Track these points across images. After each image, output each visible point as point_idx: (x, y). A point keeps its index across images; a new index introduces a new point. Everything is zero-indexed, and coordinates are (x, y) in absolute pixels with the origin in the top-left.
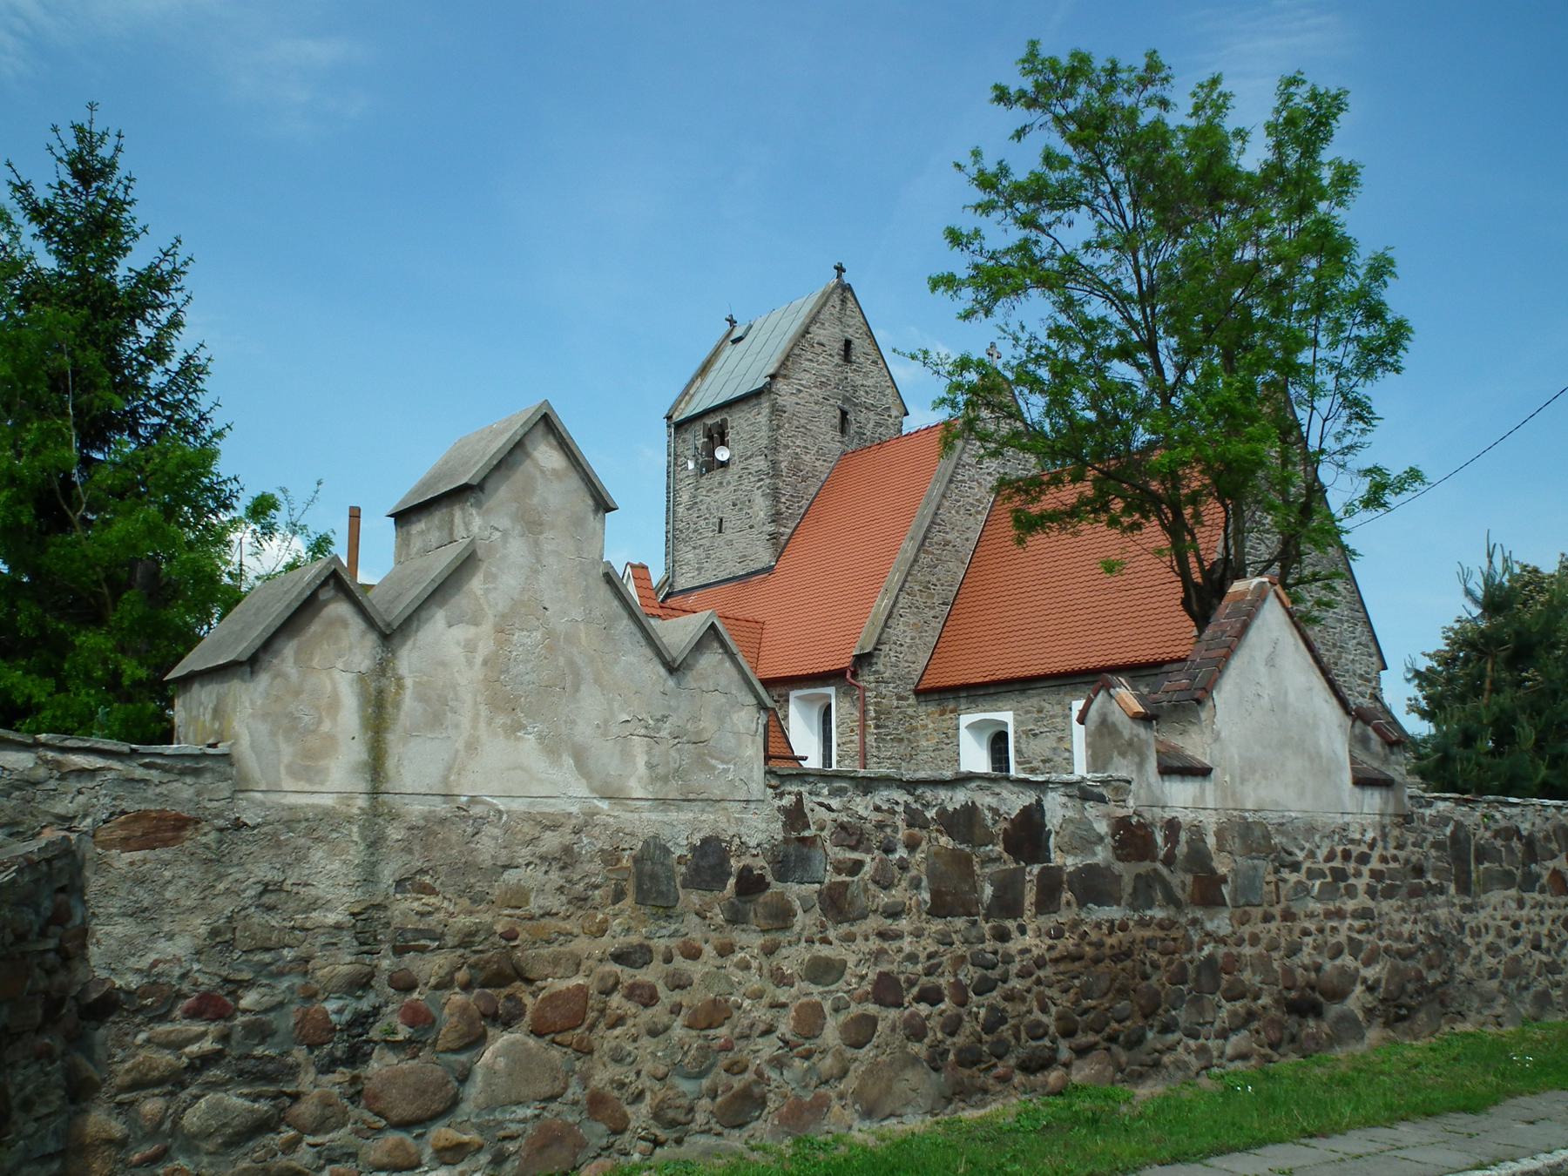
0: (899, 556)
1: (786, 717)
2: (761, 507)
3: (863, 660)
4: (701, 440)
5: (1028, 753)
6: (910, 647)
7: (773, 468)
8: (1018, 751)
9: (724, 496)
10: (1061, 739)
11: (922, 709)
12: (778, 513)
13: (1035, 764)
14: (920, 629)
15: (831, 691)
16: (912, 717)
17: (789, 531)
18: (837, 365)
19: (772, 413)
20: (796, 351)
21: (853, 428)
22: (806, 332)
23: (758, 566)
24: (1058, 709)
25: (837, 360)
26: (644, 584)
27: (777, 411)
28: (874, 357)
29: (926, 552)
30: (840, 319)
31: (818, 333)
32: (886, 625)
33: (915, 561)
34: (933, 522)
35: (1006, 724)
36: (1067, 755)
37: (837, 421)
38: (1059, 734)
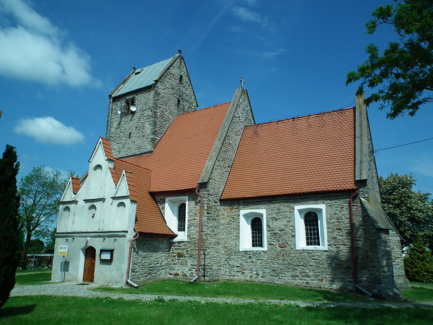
0: (214, 146)
1: (163, 208)
2: (148, 129)
3: (203, 185)
4: (124, 104)
5: (270, 224)
6: (219, 182)
7: (155, 114)
8: (268, 226)
9: (133, 124)
11: (222, 207)
12: (156, 131)
13: (276, 231)
14: (222, 175)
15: (186, 198)
16: (218, 210)
17: (159, 139)
18: (178, 83)
19: (155, 94)
20: (165, 74)
21: (181, 107)
22: (169, 69)
24: (287, 209)
25: (178, 81)
27: (157, 94)
28: (189, 84)
29: (224, 146)
30: (179, 68)
31: (172, 70)
32: (212, 173)
33: (221, 149)
34: (226, 135)
37: (176, 103)
38: (288, 219)
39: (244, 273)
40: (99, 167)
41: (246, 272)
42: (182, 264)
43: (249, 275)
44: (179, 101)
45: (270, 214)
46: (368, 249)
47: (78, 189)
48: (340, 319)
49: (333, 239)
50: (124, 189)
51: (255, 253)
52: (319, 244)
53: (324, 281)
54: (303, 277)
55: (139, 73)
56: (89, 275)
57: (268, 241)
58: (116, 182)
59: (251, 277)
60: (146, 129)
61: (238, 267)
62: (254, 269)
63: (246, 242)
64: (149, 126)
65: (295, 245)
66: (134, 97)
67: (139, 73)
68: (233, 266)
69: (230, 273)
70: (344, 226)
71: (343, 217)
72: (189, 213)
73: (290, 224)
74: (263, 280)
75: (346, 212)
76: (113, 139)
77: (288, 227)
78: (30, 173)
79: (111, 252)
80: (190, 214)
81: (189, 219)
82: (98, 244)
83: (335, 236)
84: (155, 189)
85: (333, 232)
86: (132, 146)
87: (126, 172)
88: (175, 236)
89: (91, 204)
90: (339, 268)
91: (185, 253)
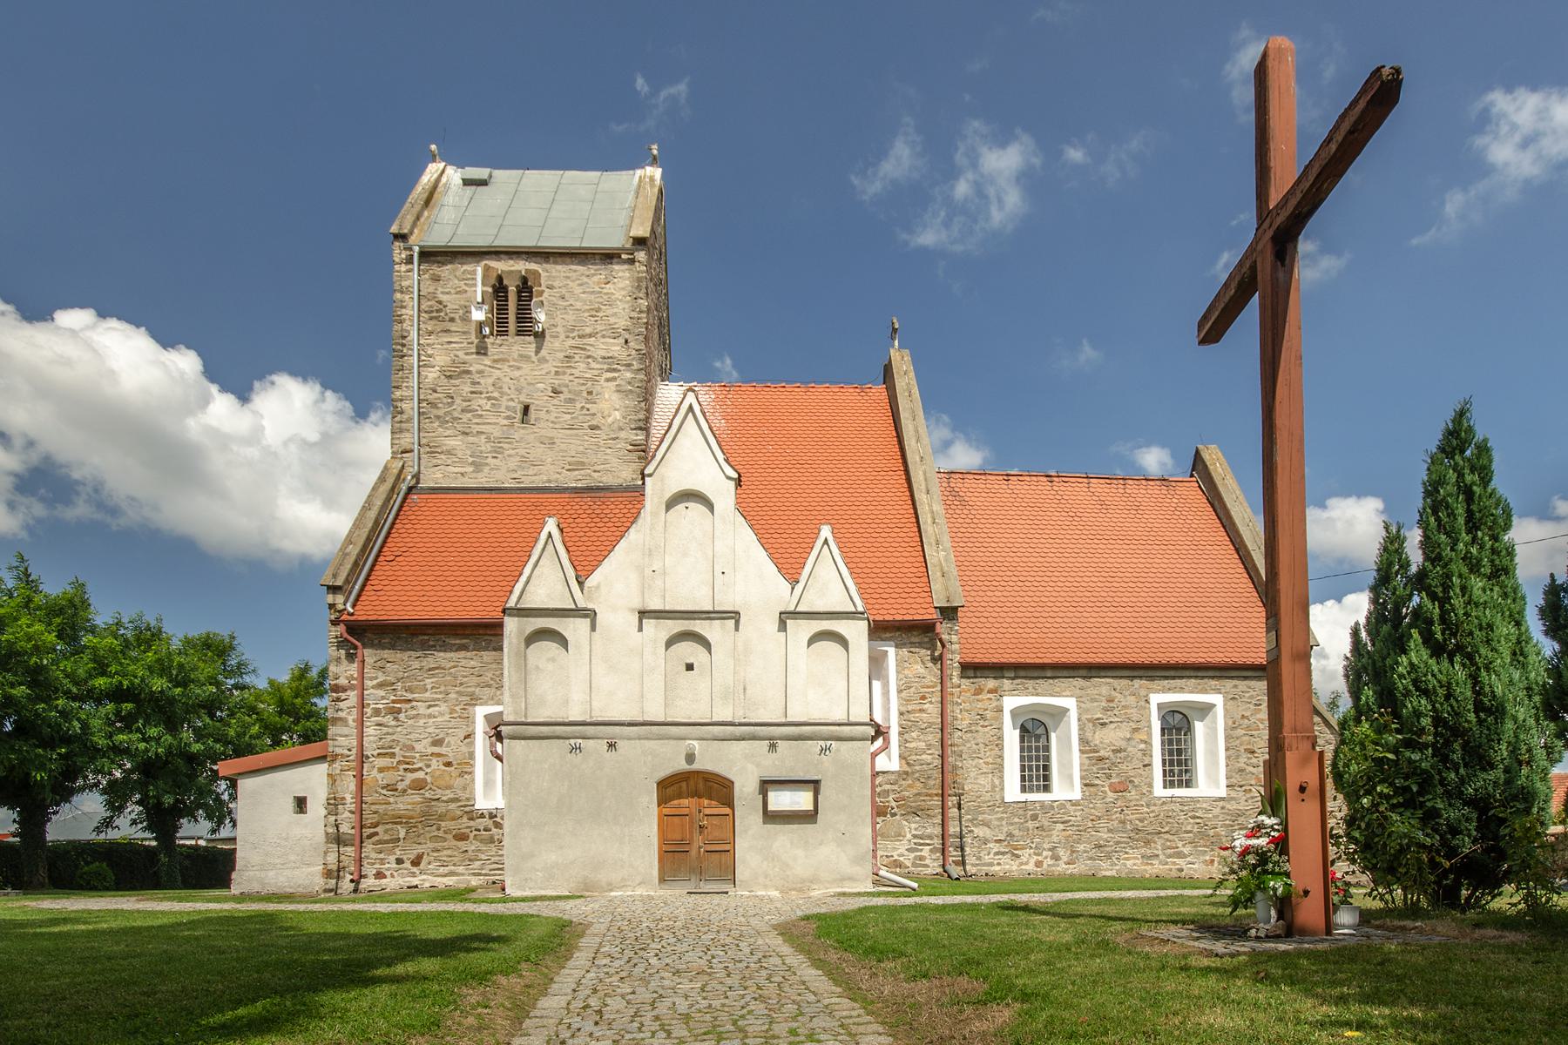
5: (1089, 735)
10: (1136, 730)
13: (1102, 753)
36: (1142, 746)
39: (1018, 856)
41: (1025, 854)
43: (1032, 861)
45: (1087, 711)
52: (1188, 784)
54: (1170, 856)
59: (1039, 864)
62: (1046, 846)
64: (615, 397)
69: (979, 858)
72: (900, 691)
73: (1138, 736)
74: (1071, 869)
76: (440, 413)
79: (815, 785)
80: (904, 694)
81: (904, 709)
85: (1238, 757)
91: (894, 804)
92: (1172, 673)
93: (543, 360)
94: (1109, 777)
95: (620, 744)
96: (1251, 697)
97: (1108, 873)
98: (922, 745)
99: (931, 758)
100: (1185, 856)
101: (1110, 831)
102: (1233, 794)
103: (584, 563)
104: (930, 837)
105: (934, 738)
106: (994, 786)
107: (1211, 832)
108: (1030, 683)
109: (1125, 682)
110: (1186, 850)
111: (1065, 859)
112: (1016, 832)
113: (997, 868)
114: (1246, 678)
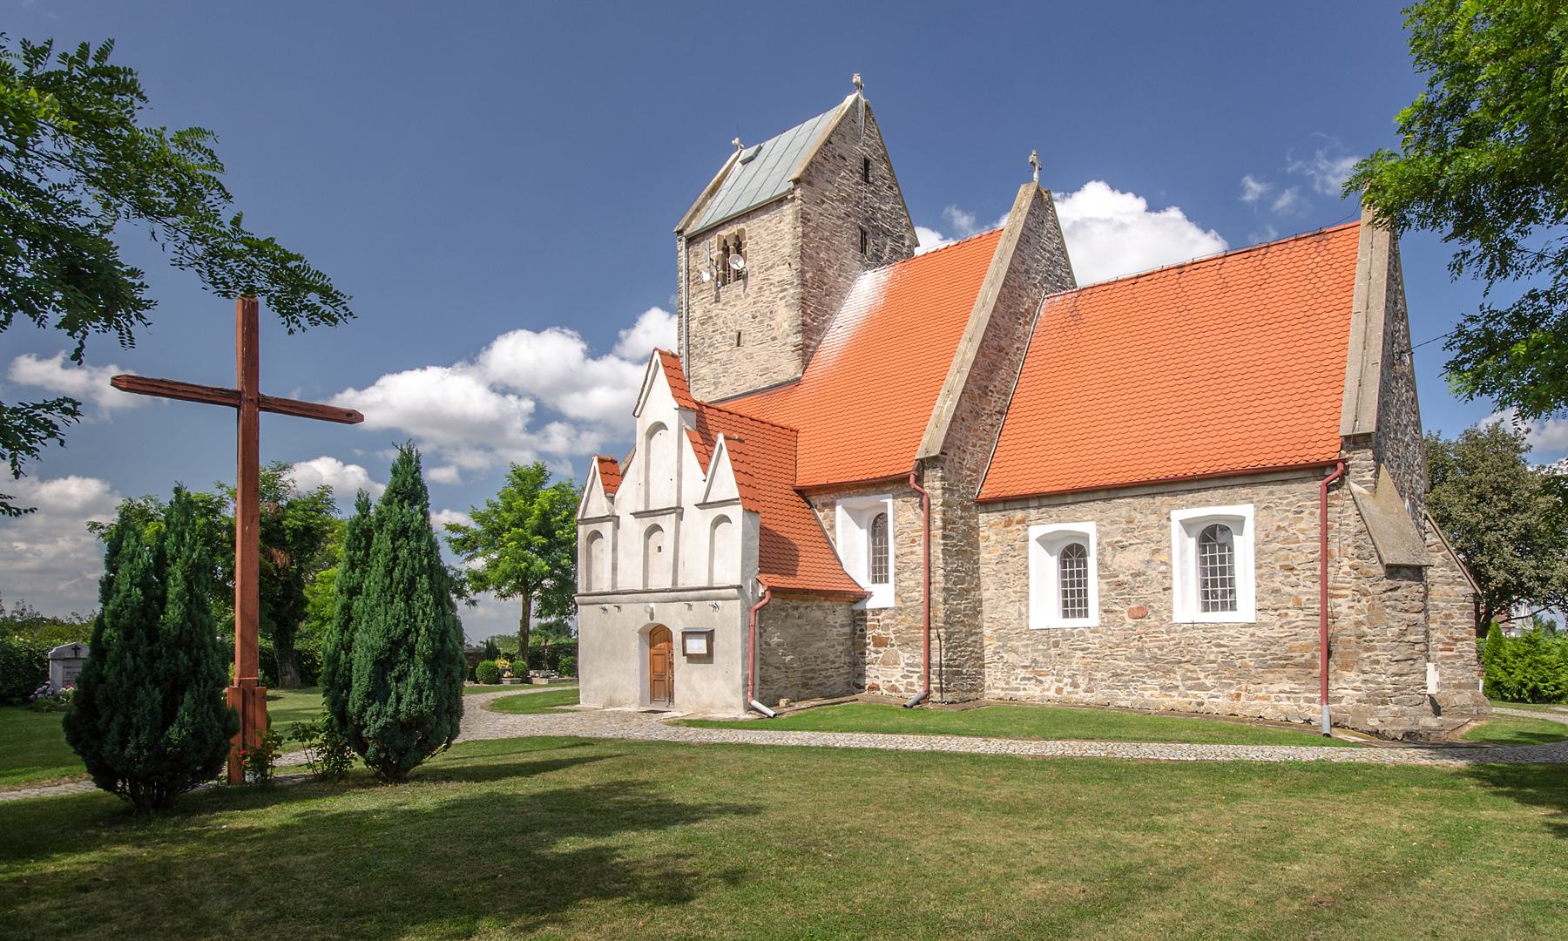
0: (957, 359)
1: (832, 527)
4: (717, 253)
5: (1108, 559)
8: (1102, 565)
10: (1156, 551)
18: (857, 183)
23: (782, 378)
25: (857, 178)
26: (676, 373)
35: (1086, 537)
36: (1163, 568)
40: (660, 426)
41: (1047, 680)
42: (884, 663)
44: (864, 233)
45: (1107, 534)
46: (1361, 617)
47: (617, 486)
48: (1055, 712)
49: (1269, 598)
50: (726, 484)
51: (1067, 635)
52: (1233, 607)
53: (1243, 699)
54: (1190, 688)
55: (751, 159)
56: (660, 686)
57: (1101, 604)
58: (704, 465)
59: (1059, 691)
60: (778, 319)
61: (1025, 667)
63: (1045, 609)
65: (1170, 611)
66: (742, 231)
67: (751, 159)
68: (1014, 667)
70: (1303, 559)
71: (1302, 537)
74: (1089, 698)
75: (1309, 524)
77: (1153, 565)
78: (1447, 239)
79: (709, 636)
82: (675, 618)
83: (1277, 585)
84: (805, 478)
85: (1272, 576)
86: (747, 366)
87: (726, 438)
88: (863, 596)
89: (649, 521)
90: (1284, 666)
92: (1195, 486)
93: (747, 296)
94: (1128, 602)
95: (623, 606)
96: (1291, 504)
97: (1123, 704)
98: (912, 583)
99: (919, 595)
100: (1206, 689)
101: (1128, 659)
102: (1265, 618)
103: (611, 489)
104: (917, 666)
105: (921, 577)
106: (1020, 614)
107: (1238, 663)
108: (1054, 510)
109: (1144, 500)
110: (1208, 683)
111: (1083, 686)
112: (1040, 659)
113: (1022, 693)
114: (1285, 482)
